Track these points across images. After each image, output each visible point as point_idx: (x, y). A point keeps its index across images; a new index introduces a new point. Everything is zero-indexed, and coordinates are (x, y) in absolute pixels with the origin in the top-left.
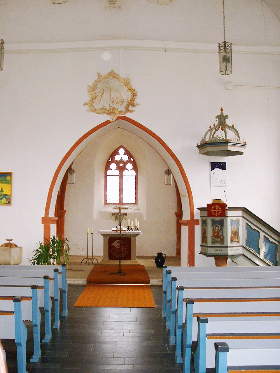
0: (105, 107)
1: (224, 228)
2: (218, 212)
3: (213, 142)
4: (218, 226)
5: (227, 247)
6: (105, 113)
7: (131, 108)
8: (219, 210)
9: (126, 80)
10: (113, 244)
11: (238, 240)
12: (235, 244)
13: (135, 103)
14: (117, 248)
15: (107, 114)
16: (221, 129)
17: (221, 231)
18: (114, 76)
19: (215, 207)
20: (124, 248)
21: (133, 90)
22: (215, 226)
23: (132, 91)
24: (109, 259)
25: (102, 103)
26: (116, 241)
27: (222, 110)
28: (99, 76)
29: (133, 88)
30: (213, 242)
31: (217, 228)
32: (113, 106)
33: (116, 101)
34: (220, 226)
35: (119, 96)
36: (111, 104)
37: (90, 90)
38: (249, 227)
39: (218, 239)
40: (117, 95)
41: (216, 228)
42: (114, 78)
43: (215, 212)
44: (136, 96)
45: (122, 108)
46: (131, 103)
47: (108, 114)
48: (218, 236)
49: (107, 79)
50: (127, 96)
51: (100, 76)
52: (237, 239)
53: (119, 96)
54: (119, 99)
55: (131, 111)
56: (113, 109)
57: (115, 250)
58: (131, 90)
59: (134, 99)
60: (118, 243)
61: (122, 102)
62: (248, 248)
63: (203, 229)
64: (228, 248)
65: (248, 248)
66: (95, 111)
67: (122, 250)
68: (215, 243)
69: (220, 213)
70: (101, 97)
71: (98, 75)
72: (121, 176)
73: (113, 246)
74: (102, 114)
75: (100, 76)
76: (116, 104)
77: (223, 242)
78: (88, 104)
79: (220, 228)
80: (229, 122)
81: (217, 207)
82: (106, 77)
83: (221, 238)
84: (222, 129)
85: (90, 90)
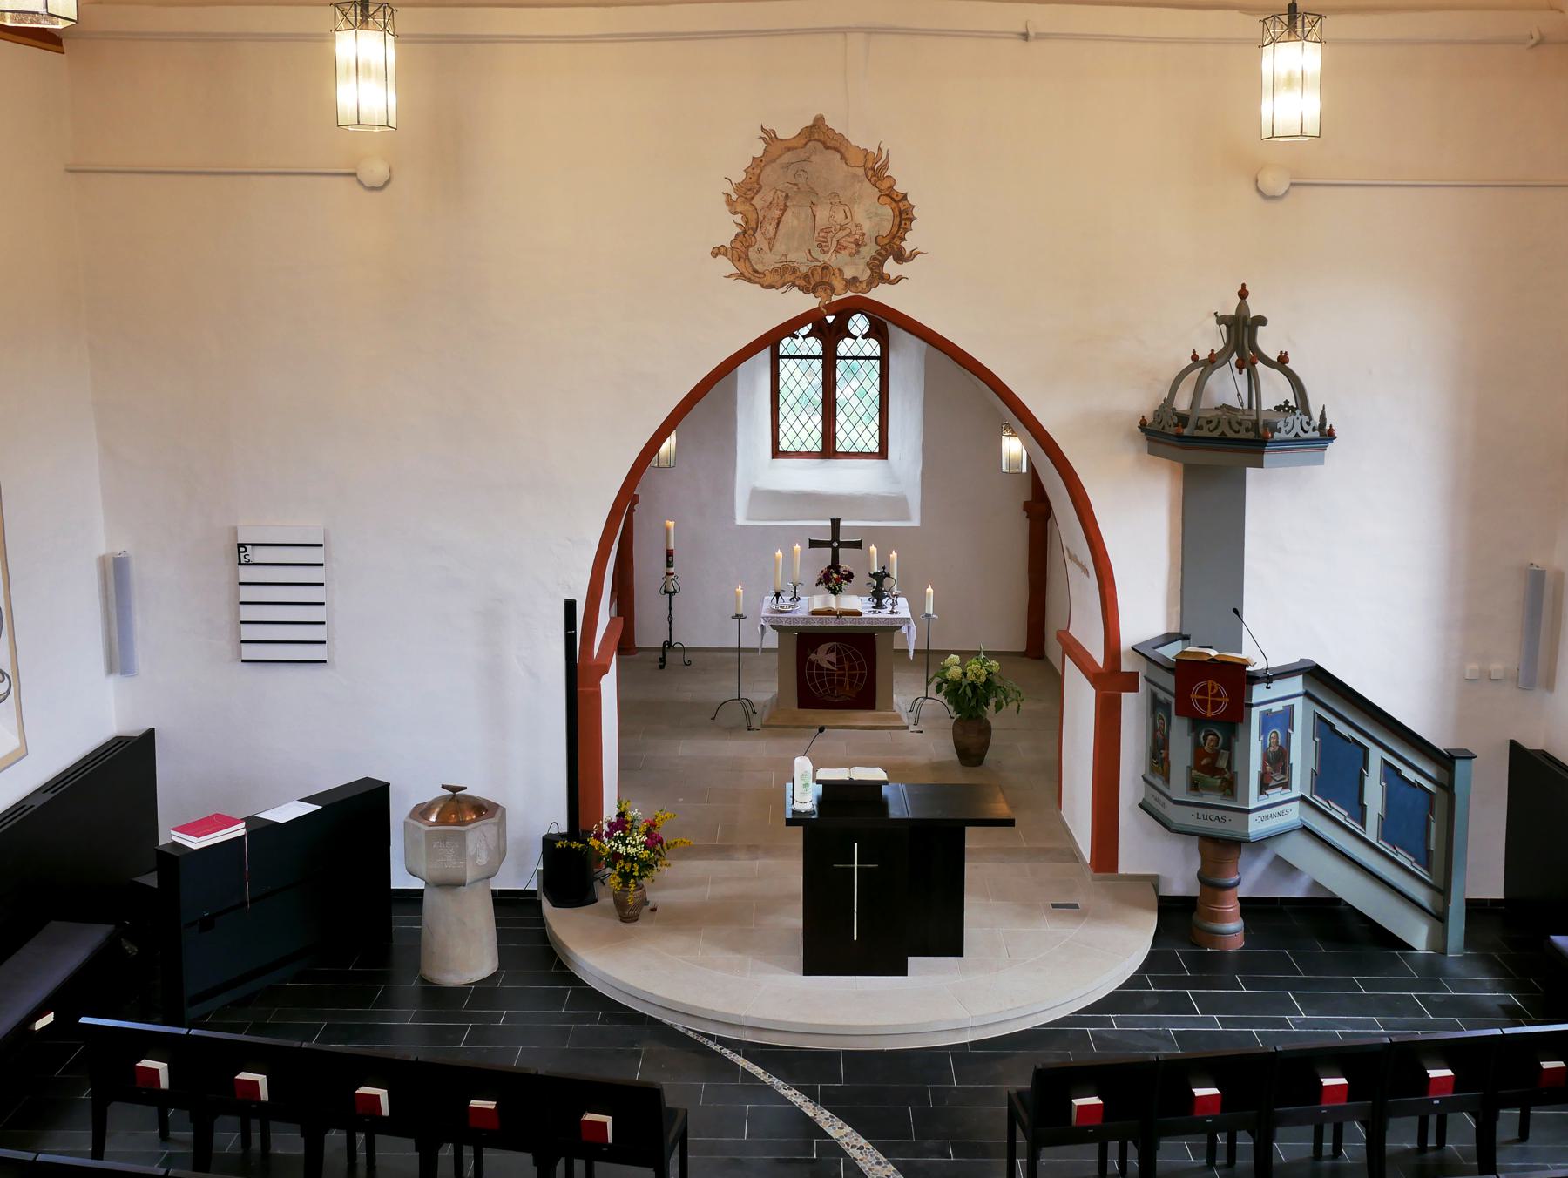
0: (796, 264)
1: (1237, 743)
2: (1216, 705)
3: (1205, 433)
4: (1215, 734)
5: (1248, 811)
6: (794, 285)
7: (890, 267)
8: (1218, 699)
9: (871, 157)
10: (813, 657)
11: (1286, 780)
12: (1275, 795)
13: (908, 246)
14: (828, 669)
15: (801, 289)
16: (1237, 367)
17: (1225, 754)
18: (822, 139)
19: (1206, 686)
20: (852, 668)
21: (897, 199)
22: (1203, 734)
23: (895, 201)
24: (802, 705)
25: (780, 247)
26: (822, 646)
27: (1243, 294)
28: (768, 138)
29: (899, 188)
30: (1194, 786)
31: (1212, 740)
32: (824, 258)
33: (835, 239)
34: (1221, 733)
35: (847, 221)
36: (816, 253)
37: (734, 197)
38: (1328, 728)
39: (1213, 780)
40: (840, 217)
41: (1208, 741)
42: (827, 148)
43: (1203, 703)
44: (911, 220)
45: (856, 268)
46: (893, 248)
47: (805, 290)
48: (1212, 770)
49: (802, 154)
50: (871, 217)
51: (770, 137)
52: (1282, 777)
53: (847, 221)
54: (848, 231)
55: (892, 277)
56: (824, 271)
57: (820, 676)
58: (892, 198)
59: (902, 230)
60: (830, 651)
61: (858, 245)
62: (1319, 801)
63: (1155, 730)
64: (1251, 816)
65: (1319, 801)
66: (757, 280)
67: (844, 675)
68: (1201, 790)
69: (1222, 708)
70: (778, 224)
71: (763, 139)
72: (829, 360)
73: (812, 664)
74: (783, 289)
75: (771, 138)
76: (837, 251)
77: (1230, 793)
78: (729, 254)
79: (1221, 742)
80: (1268, 342)
81: (1213, 688)
82: (794, 143)
83: (1226, 776)
84: (1240, 366)
85: (734, 197)
